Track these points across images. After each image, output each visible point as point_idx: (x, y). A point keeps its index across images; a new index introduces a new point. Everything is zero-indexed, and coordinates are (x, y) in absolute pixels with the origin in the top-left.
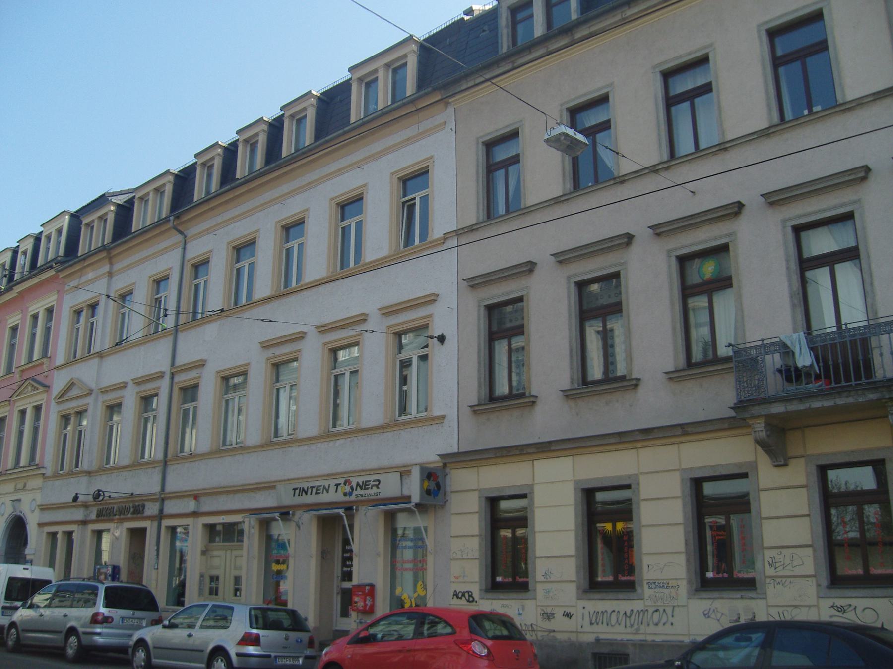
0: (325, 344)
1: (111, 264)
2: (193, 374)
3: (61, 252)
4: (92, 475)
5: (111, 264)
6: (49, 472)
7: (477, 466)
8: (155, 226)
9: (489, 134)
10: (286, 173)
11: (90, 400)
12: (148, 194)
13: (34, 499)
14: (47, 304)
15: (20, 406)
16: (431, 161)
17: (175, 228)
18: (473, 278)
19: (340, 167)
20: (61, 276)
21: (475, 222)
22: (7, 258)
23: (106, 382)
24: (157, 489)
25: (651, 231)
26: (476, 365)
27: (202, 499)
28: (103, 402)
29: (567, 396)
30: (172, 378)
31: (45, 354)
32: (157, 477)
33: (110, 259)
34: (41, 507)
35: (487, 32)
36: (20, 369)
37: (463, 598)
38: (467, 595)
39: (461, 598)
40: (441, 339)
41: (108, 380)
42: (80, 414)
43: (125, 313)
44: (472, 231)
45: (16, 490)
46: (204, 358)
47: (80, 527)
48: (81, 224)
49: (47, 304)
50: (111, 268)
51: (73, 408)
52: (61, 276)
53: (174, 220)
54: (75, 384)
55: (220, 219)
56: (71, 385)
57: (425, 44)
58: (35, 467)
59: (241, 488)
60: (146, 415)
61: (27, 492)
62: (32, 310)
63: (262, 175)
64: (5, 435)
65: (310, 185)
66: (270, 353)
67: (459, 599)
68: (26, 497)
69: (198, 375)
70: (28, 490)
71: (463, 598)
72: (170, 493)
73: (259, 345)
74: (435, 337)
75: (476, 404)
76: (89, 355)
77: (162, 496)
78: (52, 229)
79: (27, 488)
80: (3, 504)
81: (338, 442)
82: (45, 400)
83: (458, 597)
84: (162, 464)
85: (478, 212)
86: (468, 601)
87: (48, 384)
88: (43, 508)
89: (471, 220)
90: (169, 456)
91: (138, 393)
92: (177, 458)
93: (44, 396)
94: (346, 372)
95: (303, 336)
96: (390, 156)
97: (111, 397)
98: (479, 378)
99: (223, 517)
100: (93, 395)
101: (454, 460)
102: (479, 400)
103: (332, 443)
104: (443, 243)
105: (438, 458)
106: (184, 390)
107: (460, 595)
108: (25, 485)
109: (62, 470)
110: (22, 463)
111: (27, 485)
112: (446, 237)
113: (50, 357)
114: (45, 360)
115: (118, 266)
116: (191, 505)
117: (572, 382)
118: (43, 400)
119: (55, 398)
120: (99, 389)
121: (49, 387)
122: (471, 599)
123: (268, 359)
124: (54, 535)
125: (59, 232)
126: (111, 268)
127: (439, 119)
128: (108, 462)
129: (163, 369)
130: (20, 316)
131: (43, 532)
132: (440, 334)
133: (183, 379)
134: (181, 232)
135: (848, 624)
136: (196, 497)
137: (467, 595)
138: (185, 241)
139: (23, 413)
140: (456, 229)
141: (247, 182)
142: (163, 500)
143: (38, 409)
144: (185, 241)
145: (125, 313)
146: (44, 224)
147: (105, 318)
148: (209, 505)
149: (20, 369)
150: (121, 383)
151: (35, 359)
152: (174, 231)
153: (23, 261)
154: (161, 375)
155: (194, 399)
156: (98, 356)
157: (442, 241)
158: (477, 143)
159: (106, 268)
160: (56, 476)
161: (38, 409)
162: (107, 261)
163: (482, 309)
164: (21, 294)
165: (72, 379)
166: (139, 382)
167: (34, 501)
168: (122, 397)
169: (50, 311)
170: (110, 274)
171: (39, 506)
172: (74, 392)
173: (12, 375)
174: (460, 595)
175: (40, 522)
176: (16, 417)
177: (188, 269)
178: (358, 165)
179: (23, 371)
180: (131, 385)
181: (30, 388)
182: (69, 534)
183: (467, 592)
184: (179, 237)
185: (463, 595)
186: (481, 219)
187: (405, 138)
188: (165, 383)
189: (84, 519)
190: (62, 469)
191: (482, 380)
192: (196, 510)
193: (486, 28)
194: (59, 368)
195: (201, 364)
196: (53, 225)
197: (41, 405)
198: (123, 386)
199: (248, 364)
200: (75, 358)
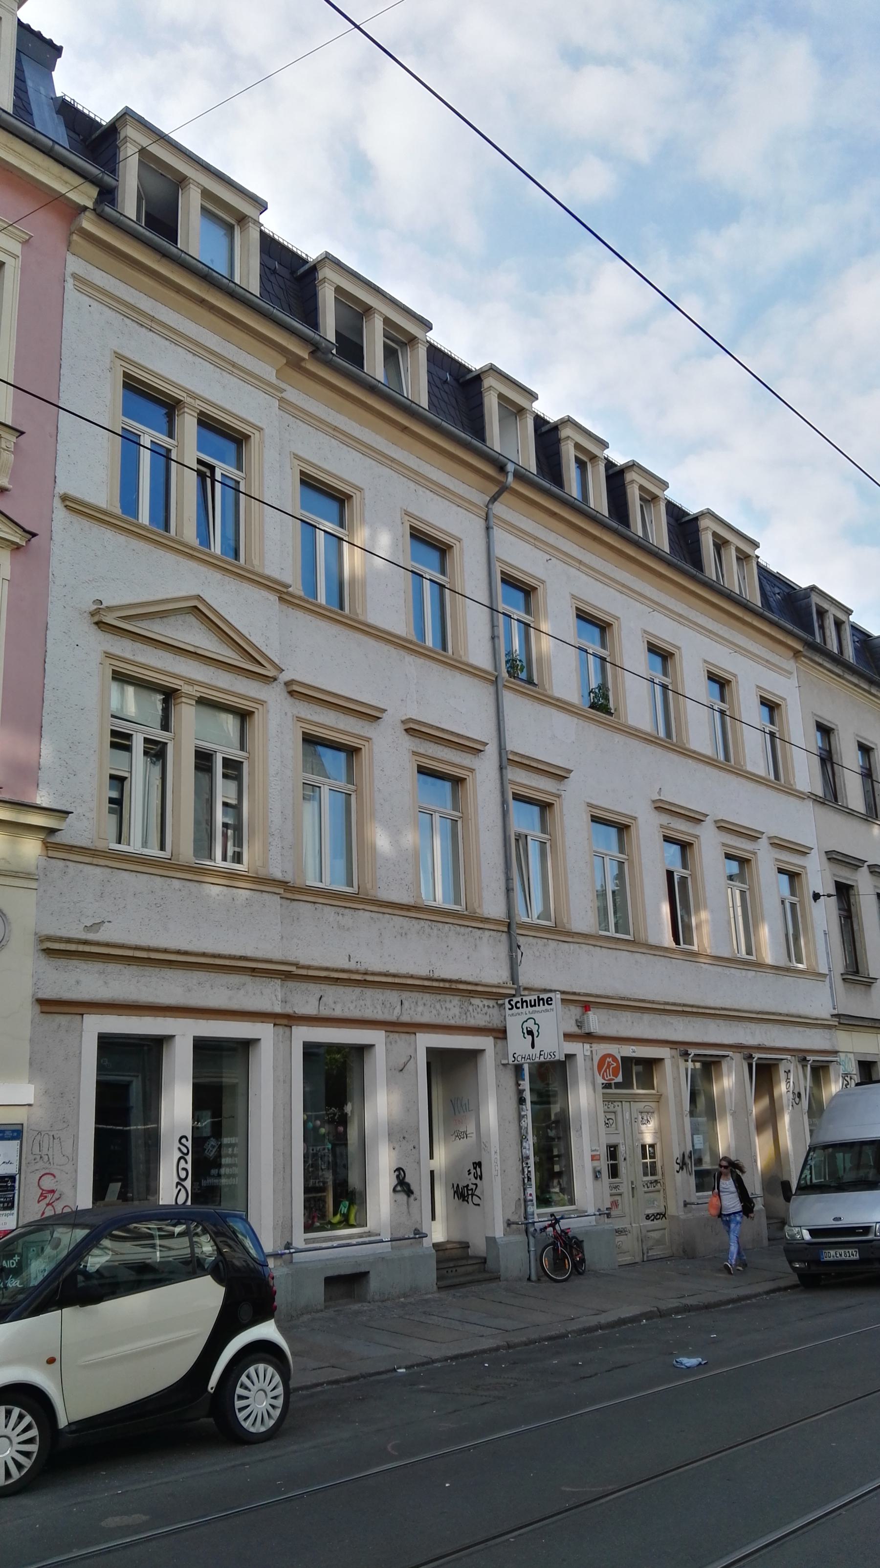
10: (553, 515)
59: (662, 1007)
104: (804, 799)
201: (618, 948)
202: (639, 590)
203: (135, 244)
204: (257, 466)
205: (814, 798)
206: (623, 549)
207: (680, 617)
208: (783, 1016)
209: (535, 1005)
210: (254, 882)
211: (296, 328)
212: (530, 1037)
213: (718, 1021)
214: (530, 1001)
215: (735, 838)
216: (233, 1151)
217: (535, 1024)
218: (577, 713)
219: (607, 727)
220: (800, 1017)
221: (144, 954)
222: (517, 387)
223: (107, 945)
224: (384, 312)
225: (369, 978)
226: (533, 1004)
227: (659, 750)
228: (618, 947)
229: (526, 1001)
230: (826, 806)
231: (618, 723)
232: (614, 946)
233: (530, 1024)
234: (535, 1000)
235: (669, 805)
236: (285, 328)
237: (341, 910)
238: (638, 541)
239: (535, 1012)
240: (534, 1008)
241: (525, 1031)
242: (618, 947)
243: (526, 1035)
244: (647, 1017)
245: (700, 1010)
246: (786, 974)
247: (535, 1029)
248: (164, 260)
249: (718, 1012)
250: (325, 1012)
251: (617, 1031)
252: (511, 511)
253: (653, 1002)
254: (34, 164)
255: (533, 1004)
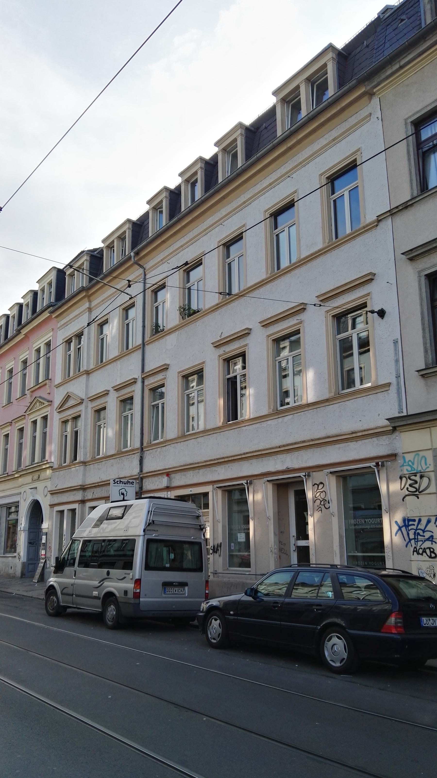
0: (268, 336)
1: (90, 302)
2: (159, 377)
3: (53, 300)
4: (87, 464)
5: (90, 302)
6: (56, 466)
7: (429, 427)
8: (121, 264)
9: (418, 112)
10: (223, 198)
11: (82, 408)
12: (113, 242)
13: (46, 487)
14: (46, 340)
15: (32, 418)
16: (359, 153)
17: (136, 263)
18: (411, 250)
19: (271, 182)
20: (53, 317)
21: (409, 198)
22: (2, 322)
23: (93, 392)
24: (136, 471)
25: (404, 257)
26: (420, 332)
27: (173, 476)
28: (92, 408)
29: (422, 376)
30: (143, 382)
31: (47, 377)
32: (136, 462)
33: (89, 297)
34: (51, 492)
35: (407, 20)
36: (31, 390)
37: (424, 554)
38: (428, 551)
39: (422, 554)
40: (382, 313)
41: (94, 391)
42: (76, 418)
43: (103, 338)
44: (406, 207)
45: (33, 481)
46: (373, 272)
47: (80, 505)
48: (65, 275)
49: (46, 340)
50: (90, 305)
51: (70, 415)
52: (53, 317)
53: (134, 257)
54: (71, 396)
55: (171, 250)
56: (68, 397)
57: (342, 51)
58: (6, 475)
59: (204, 464)
60: (98, 423)
61: (41, 482)
62: (36, 346)
63: (203, 202)
64: (9, 447)
65: (245, 204)
66: (221, 351)
67: (420, 556)
68: (40, 485)
69: (163, 377)
70: (41, 481)
71: (424, 554)
72: (147, 473)
73: (212, 346)
74: (376, 312)
75: (424, 367)
76: (79, 373)
77: (141, 476)
78: (45, 283)
79: (41, 478)
80: (24, 492)
81: (286, 419)
82: (49, 412)
83: (418, 554)
84: (139, 451)
85: (412, 188)
86: (430, 557)
87: (51, 400)
88: (53, 493)
89: (405, 196)
90: (145, 444)
91: (117, 398)
92: (150, 445)
93: (49, 409)
94: (129, 414)
95: (108, 393)
96: (317, 160)
97: (98, 404)
98: (425, 344)
99: (191, 489)
100: (84, 403)
101: (404, 423)
102: (426, 364)
103: (280, 419)
104: (377, 225)
105: (387, 423)
106: (153, 390)
107: (421, 551)
108: (39, 477)
109: (65, 463)
110: (36, 461)
111: (40, 476)
112: (379, 220)
113: (51, 379)
114: (47, 381)
115: (94, 304)
116: (164, 482)
117: (330, 392)
118: (48, 411)
119: (56, 409)
120: (88, 398)
121: (52, 401)
122: (433, 555)
123: (220, 356)
124: (62, 512)
125: (50, 284)
126: (90, 305)
127: (364, 113)
128: (126, 446)
129: (136, 376)
130: (13, 362)
131: (53, 511)
132: (380, 309)
133: (151, 382)
134: (141, 266)
135: (420, 580)
136: (168, 475)
137: (428, 551)
138: (145, 272)
139: (35, 422)
140: (389, 209)
141: (190, 211)
142: (142, 479)
143: (45, 418)
144: (145, 272)
145: (103, 338)
146: (39, 280)
147: (89, 343)
148: (178, 479)
149: (31, 390)
150: (132, 379)
151: (40, 381)
152: (136, 266)
153: (27, 314)
154: (134, 381)
155: (162, 395)
156: (86, 373)
157: (376, 224)
158: (406, 124)
159: (87, 305)
160: (61, 468)
161: (45, 418)
162: (86, 299)
163: (423, 279)
164: (27, 336)
165: (68, 393)
166: (118, 389)
167: (46, 488)
168: (246, 345)
169: (48, 344)
170: (90, 310)
171: (49, 491)
172: (71, 403)
173: (25, 396)
174: (421, 551)
175: (51, 504)
176: (16, 433)
177: (149, 293)
178: (287, 175)
179: (32, 392)
180: (112, 391)
181: (38, 404)
182: (73, 511)
183: (427, 548)
184: (141, 271)
185: (424, 551)
186: (415, 194)
187: (331, 139)
188: (138, 387)
189: (83, 499)
190: (65, 462)
191: (428, 345)
192: (168, 486)
193: (403, 17)
194: (58, 386)
195: (165, 368)
196: (45, 280)
197: (47, 416)
198: (106, 393)
199: (204, 363)
200: (69, 376)
201: (279, 417)
202: (218, 219)
203: (59, 310)
204: (324, 195)
205: (389, 214)
206: (193, 217)
207: (245, 203)
208: (307, 442)
209: (126, 484)
210: (78, 464)
211: (250, 163)
212: (123, 496)
213: (251, 461)
214: (124, 482)
215: (276, 326)
216: (241, 527)
217: (125, 491)
218: (175, 330)
219: (192, 323)
220: (329, 437)
221: (223, 460)
222: (323, 54)
223: (59, 490)
224: (163, 197)
225: (99, 484)
226: (125, 483)
227: (225, 308)
228: (187, 439)
229: (122, 482)
230: (415, 205)
231: (204, 312)
232: (185, 440)
233: (123, 491)
234: (126, 482)
235: (219, 342)
236: (306, 124)
237: (99, 463)
238: (291, 132)
239: (126, 486)
240: (125, 485)
241: (120, 493)
242: (187, 439)
243: (121, 495)
244: (202, 471)
245: (230, 459)
246: (328, 404)
247: (125, 493)
248: (61, 308)
249: (236, 458)
250: (94, 497)
251: (185, 482)
252: (148, 263)
253: (198, 463)
254: (35, 323)
255: (125, 483)
